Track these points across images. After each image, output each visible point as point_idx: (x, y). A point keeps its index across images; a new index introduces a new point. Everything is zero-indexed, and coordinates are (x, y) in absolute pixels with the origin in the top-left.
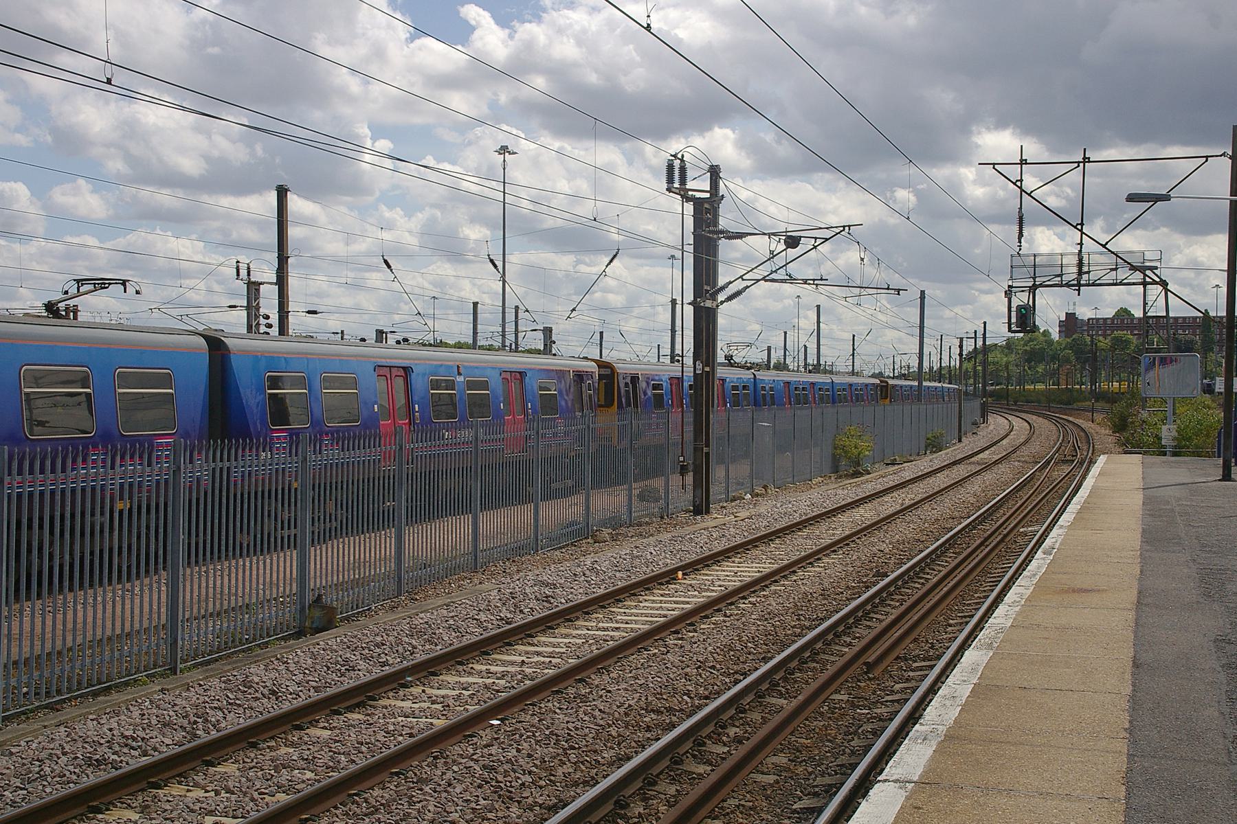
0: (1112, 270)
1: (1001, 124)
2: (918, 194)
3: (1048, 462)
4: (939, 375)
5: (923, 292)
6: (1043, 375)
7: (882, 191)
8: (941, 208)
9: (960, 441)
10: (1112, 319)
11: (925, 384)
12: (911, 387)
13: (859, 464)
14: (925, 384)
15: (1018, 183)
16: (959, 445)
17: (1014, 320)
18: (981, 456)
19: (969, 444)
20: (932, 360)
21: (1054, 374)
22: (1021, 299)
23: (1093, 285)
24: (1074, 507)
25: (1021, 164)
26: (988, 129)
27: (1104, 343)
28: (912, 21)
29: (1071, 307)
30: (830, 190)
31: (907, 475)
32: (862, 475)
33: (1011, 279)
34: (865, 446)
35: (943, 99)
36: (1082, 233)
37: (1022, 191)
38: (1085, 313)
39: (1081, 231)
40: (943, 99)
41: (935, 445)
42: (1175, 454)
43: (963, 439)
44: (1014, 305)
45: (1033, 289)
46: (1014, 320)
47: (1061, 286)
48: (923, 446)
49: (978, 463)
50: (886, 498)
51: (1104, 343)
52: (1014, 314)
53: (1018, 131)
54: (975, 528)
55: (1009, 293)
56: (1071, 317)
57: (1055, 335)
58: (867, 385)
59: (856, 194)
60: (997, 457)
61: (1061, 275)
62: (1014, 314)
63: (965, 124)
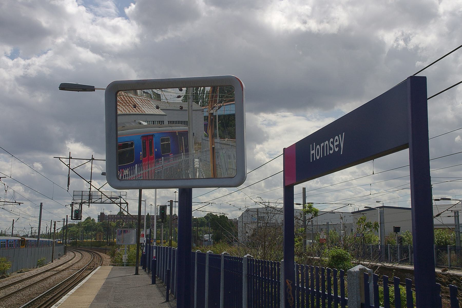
0: (100, 199)
1: (77, 141)
2: (43, 165)
3: (83, 269)
4: (45, 236)
5: (41, 204)
6: (91, 236)
7: (30, 162)
8: (49, 170)
9: (52, 262)
10: (117, 215)
11: (40, 239)
12: (35, 241)
13: (4, 273)
14: (40, 239)
15: (69, 166)
16: (52, 264)
17: (73, 215)
18: (59, 268)
19: (56, 263)
20: (43, 231)
21: (95, 235)
22: (76, 207)
23: (103, 203)
24: (76, 288)
25: (70, 159)
26: (71, 143)
27: (114, 224)
28: (40, 100)
29: (103, 210)
30: (7, 161)
31: (24, 277)
32: (5, 277)
33: (73, 199)
34: (8, 265)
35: (55, 129)
36: (91, 185)
37: (70, 168)
38: (107, 213)
39: (90, 184)
40: (55, 129)
41: (41, 264)
42: (127, 265)
43: (54, 261)
44: (74, 210)
45: (81, 204)
46: (73, 215)
47: (101, 203)
48: (36, 264)
49: (56, 271)
50: (12, 287)
51: (114, 224)
52: (74, 213)
53: (82, 144)
54: (44, 297)
55: (72, 205)
56: (102, 214)
57: (96, 220)
58: (15, 240)
59: (17, 163)
60: (64, 268)
61: (101, 198)
62: (74, 213)
63: (64, 139)
